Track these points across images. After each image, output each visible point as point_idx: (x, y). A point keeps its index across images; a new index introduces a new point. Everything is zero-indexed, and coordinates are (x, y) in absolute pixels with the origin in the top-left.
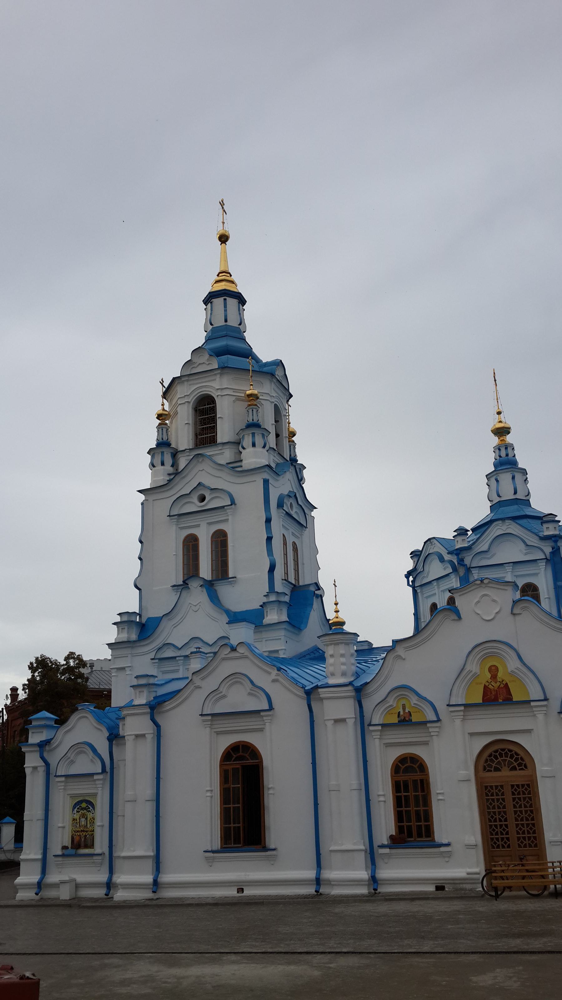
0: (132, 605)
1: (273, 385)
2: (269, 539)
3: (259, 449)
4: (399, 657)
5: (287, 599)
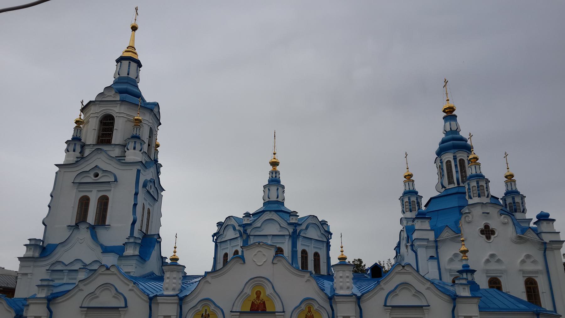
0: (39, 235)
1: (151, 117)
2: (135, 205)
3: (137, 151)
4: (207, 282)
5: (139, 241)
